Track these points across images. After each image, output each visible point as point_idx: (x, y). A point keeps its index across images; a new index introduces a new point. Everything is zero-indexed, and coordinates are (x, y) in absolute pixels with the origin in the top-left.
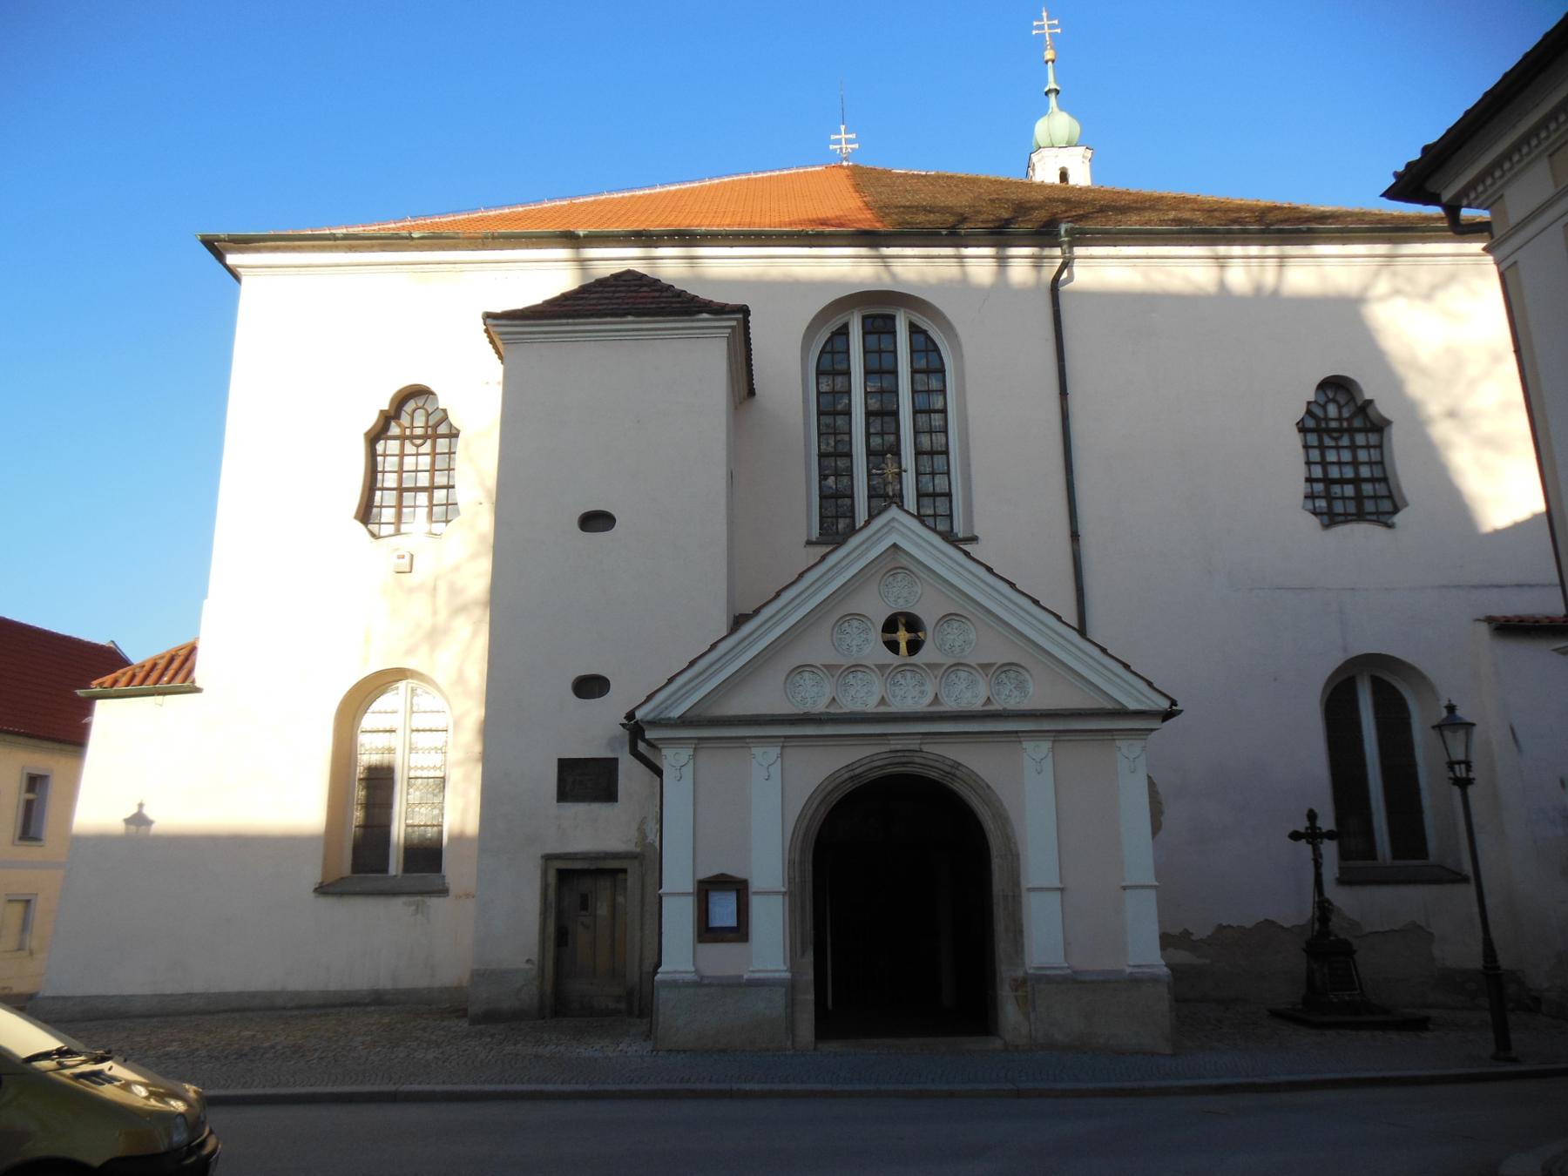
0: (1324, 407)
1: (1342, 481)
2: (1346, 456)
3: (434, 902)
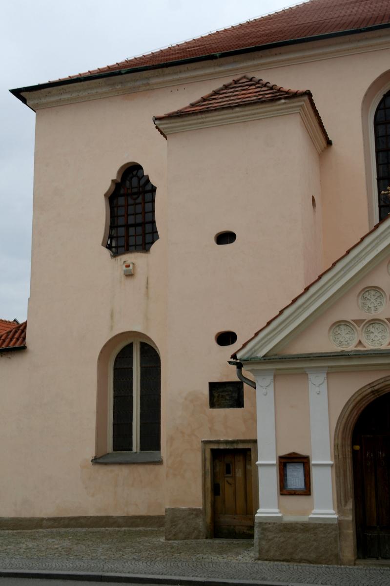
3: (157, 467)
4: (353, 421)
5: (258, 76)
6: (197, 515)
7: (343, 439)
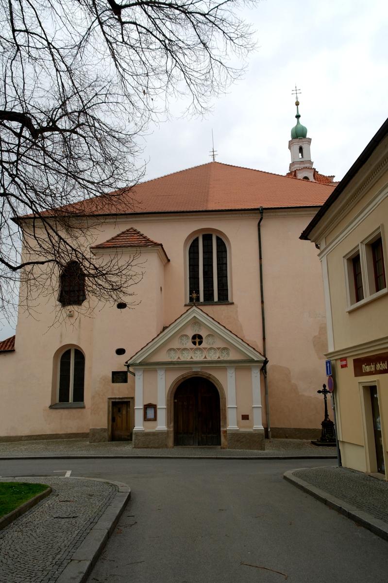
4: (174, 391)
5: (139, 229)
6: (105, 431)
7: (171, 397)
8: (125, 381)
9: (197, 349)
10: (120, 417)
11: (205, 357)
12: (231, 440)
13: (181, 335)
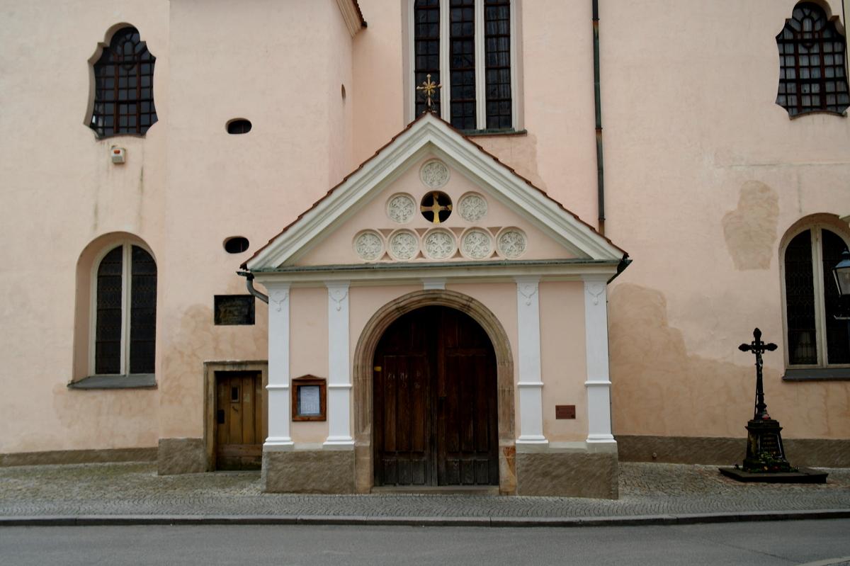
0: (801, 23)
1: (811, 81)
2: (815, 61)
3: (150, 393)
6: (197, 447)
7: (364, 359)
8: (249, 320)
9: (435, 231)
10: (236, 410)
11: (458, 254)
12: (527, 471)
13: (389, 191)
